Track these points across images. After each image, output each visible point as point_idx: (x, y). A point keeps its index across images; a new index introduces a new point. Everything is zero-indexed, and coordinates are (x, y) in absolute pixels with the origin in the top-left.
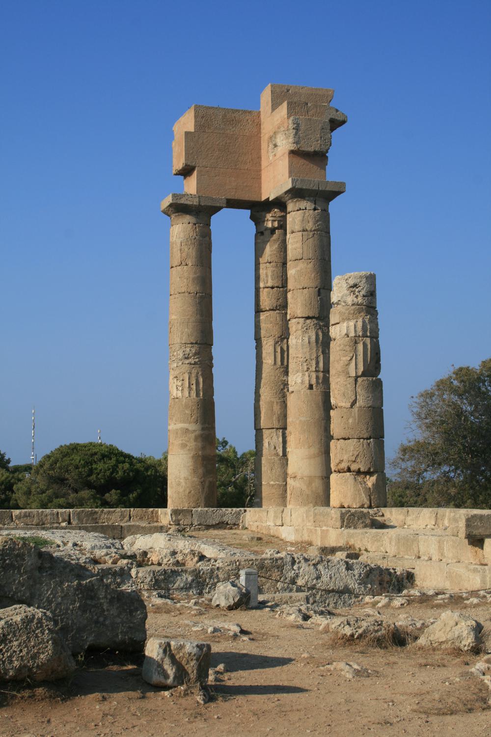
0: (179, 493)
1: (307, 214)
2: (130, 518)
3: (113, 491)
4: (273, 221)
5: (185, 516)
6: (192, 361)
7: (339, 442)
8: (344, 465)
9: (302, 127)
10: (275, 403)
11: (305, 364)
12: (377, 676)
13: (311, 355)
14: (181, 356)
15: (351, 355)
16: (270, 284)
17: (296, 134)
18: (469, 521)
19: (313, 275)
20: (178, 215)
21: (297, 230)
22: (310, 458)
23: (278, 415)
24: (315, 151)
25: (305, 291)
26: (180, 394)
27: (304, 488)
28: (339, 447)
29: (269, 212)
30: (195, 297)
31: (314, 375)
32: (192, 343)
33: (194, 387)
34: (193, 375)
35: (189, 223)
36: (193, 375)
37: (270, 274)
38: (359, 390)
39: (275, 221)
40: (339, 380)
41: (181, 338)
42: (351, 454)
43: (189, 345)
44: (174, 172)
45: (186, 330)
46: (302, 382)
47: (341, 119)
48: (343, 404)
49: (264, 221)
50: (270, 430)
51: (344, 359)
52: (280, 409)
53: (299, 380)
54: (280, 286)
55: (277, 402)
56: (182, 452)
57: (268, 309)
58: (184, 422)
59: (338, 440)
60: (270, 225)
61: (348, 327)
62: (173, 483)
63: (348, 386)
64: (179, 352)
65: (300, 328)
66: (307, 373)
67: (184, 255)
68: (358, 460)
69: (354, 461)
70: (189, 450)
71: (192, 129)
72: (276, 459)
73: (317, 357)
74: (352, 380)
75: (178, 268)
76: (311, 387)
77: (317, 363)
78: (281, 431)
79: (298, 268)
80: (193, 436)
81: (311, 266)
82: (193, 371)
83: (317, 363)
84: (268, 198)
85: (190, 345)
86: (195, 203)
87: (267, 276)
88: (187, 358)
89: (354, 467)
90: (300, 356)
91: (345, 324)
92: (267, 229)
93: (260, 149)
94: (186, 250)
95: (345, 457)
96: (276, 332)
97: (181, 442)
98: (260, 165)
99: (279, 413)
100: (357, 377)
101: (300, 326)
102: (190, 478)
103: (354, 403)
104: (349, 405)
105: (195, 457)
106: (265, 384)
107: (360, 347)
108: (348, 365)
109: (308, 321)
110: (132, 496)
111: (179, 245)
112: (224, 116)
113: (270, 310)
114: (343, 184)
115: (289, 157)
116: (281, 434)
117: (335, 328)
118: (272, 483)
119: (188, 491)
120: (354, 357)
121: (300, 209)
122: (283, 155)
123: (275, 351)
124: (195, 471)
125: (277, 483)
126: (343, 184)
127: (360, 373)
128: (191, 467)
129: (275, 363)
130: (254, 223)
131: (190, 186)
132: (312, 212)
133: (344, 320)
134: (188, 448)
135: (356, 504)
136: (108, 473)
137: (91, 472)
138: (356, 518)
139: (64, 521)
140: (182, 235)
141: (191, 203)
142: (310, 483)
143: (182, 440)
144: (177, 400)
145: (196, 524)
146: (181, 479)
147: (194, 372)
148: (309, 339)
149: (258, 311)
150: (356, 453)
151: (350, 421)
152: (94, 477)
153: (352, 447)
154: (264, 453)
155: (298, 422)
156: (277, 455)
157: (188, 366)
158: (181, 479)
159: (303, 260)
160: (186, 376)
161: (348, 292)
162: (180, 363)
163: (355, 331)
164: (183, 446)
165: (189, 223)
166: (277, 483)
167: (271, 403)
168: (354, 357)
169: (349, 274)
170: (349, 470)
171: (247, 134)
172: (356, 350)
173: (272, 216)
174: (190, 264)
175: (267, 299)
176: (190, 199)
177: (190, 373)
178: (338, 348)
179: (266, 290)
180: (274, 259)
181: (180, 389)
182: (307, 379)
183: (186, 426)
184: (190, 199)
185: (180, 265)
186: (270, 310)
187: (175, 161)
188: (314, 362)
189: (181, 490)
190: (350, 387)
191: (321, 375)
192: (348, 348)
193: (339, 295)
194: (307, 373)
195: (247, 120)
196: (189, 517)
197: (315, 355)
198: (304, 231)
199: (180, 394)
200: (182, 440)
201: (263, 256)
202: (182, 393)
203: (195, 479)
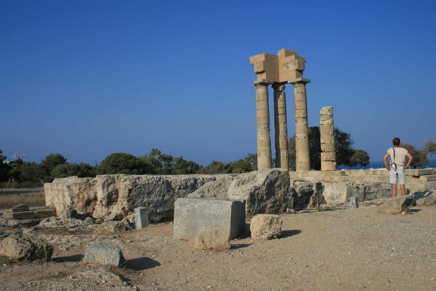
3: (135, 169)
4: (282, 88)
6: (266, 129)
8: (329, 159)
9: (300, 63)
12: (18, 239)
13: (305, 128)
14: (264, 128)
16: (281, 107)
17: (298, 65)
18: (419, 171)
22: (307, 157)
25: (303, 110)
26: (264, 139)
27: (305, 166)
28: (327, 154)
29: (280, 85)
30: (267, 110)
32: (267, 124)
34: (267, 133)
37: (281, 104)
38: (332, 138)
41: (264, 123)
46: (303, 136)
48: (328, 143)
49: (279, 88)
53: (302, 136)
56: (265, 156)
58: (265, 147)
59: (326, 152)
60: (281, 89)
61: (329, 122)
66: (304, 134)
67: (263, 98)
71: (264, 60)
73: (306, 129)
79: (300, 104)
81: (304, 103)
88: (265, 128)
89: (331, 160)
90: (302, 128)
91: (328, 121)
92: (280, 91)
96: (283, 120)
100: (331, 135)
101: (301, 120)
103: (331, 142)
104: (330, 143)
106: (281, 136)
109: (304, 119)
110: (141, 171)
113: (282, 114)
114: (310, 80)
121: (300, 87)
122: (293, 70)
126: (310, 80)
129: (284, 130)
130: (273, 89)
133: (327, 119)
136: (133, 163)
137: (128, 164)
140: (263, 92)
142: (306, 164)
144: (262, 141)
149: (285, 114)
150: (332, 156)
151: (330, 147)
152: (129, 165)
154: (281, 156)
156: (285, 157)
160: (266, 134)
161: (328, 112)
162: (263, 130)
163: (331, 123)
164: (266, 154)
167: (283, 142)
169: (328, 107)
170: (330, 161)
175: (281, 111)
179: (280, 108)
180: (282, 100)
182: (304, 135)
186: (282, 114)
187: (255, 69)
188: (306, 130)
194: (304, 134)
198: (302, 93)
199: (264, 139)
201: (279, 98)
203: (269, 164)
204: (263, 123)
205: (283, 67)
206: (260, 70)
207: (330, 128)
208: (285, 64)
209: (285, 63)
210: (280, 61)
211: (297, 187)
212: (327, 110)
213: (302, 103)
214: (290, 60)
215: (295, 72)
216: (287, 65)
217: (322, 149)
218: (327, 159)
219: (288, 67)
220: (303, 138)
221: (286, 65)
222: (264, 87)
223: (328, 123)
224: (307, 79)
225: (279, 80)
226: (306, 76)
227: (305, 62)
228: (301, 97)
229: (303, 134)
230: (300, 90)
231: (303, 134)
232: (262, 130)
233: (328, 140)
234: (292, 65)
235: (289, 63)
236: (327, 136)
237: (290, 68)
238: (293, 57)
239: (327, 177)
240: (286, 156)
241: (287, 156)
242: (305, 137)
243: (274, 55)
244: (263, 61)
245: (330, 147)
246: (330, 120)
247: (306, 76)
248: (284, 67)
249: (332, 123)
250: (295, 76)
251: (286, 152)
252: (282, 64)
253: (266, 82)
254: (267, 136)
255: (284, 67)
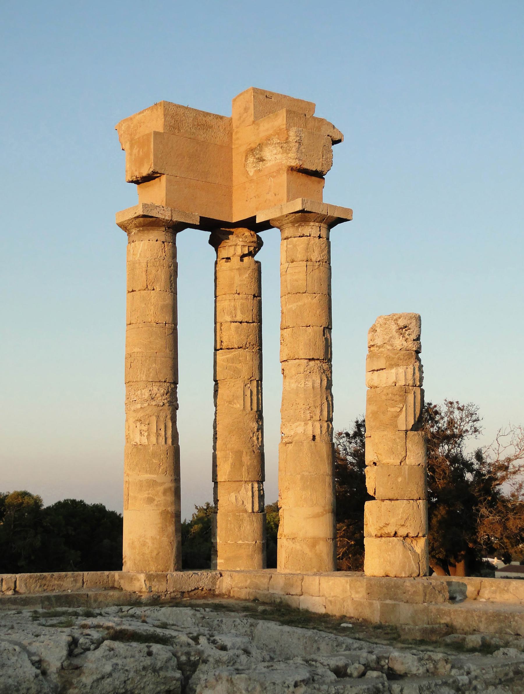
0: (143, 554)
1: (312, 242)
2: (83, 583)
5: (158, 581)
7: (383, 503)
8: (391, 530)
9: (305, 141)
10: (244, 453)
11: (308, 412)
13: (314, 401)
15: (401, 406)
16: (239, 318)
19: (318, 312)
20: (143, 230)
21: (299, 259)
22: (317, 516)
23: (247, 466)
24: (316, 171)
25: (310, 330)
27: (307, 550)
31: (318, 425)
33: (162, 432)
34: (162, 419)
35: (157, 241)
36: (162, 419)
38: (409, 445)
39: (244, 246)
40: (386, 433)
41: (147, 376)
42: (400, 517)
43: (157, 384)
44: (164, 178)
45: (154, 365)
47: (337, 138)
50: (238, 483)
51: (393, 410)
52: (250, 459)
54: (251, 321)
55: (246, 453)
57: (236, 346)
59: (383, 500)
61: (397, 374)
62: (136, 543)
63: (398, 440)
64: (143, 391)
65: (302, 371)
66: (310, 423)
68: (408, 524)
69: (403, 525)
70: (157, 505)
71: (161, 130)
72: (245, 515)
74: (402, 434)
75: (142, 292)
76: (314, 438)
77: (321, 411)
78: (250, 485)
80: (161, 489)
81: (315, 301)
82: (161, 414)
83: (321, 411)
84: (254, 218)
85: (158, 384)
86: (167, 218)
87: (235, 309)
89: (403, 532)
91: (394, 371)
93: (232, 162)
94: (154, 272)
95: (392, 521)
97: (147, 496)
98: (232, 181)
99: (249, 464)
100: (406, 431)
102: (158, 537)
105: (164, 513)
107: (410, 398)
108: (397, 416)
109: (312, 363)
111: (144, 265)
112: (195, 118)
114: (349, 211)
115: (287, 174)
116: (250, 487)
117: (379, 375)
118: (240, 542)
119: (154, 554)
120: (404, 409)
123: (245, 395)
124: (163, 530)
125: (247, 542)
127: (410, 427)
128: (160, 525)
131: (156, 195)
132: (317, 239)
133: (391, 366)
134: (156, 503)
135: (405, 573)
138: (437, 592)
139: (9, 589)
141: (163, 217)
143: (149, 494)
145: (172, 590)
146: (147, 539)
147: (162, 415)
148: (313, 384)
151: (400, 480)
153: (401, 509)
155: (299, 477)
156: (246, 511)
157: (156, 408)
158: (147, 539)
159: (307, 294)
160: (154, 419)
162: (146, 405)
164: (150, 500)
165: (157, 241)
166: (247, 542)
168: (404, 409)
171: (218, 143)
172: (405, 401)
173: (242, 241)
174: (158, 289)
176: (162, 212)
177: (158, 417)
178: (384, 397)
181: (146, 434)
183: (153, 477)
184: (162, 212)
185: (145, 290)
189: (147, 552)
190: (400, 442)
191: (325, 424)
192: (397, 398)
193: (386, 337)
194: (310, 423)
195: (219, 127)
196: (164, 583)
197: (320, 403)
199: (145, 441)
200: (149, 494)
202: (148, 439)
204: (144, 378)
205: (246, 159)
206: (145, 171)
207: (400, 401)
208: (252, 150)
209: (253, 146)
210: (238, 139)
211: (79, 675)
212: (394, 327)
213: (307, 300)
214: (271, 132)
215: (284, 177)
216: (261, 150)
217: (370, 485)
218: (387, 530)
219: (261, 160)
220: (307, 443)
221: (256, 151)
222: (158, 235)
223: (394, 379)
224: (335, 207)
225: (231, 214)
226: (333, 194)
227: (335, 142)
228: (302, 276)
229: (306, 424)
230: (299, 249)
231: (306, 424)
232: (139, 406)
233: (392, 451)
234: (275, 152)
235: (267, 144)
236: (389, 434)
237: (269, 164)
238: (280, 120)
239: (102, 660)
240: (250, 510)
241: (253, 509)
242: (314, 437)
243: (208, 114)
244: (156, 134)
245: (400, 480)
246: (401, 370)
247: (333, 194)
248: (251, 159)
249: (411, 383)
250: (283, 193)
251: (250, 493)
252: (243, 149)
253: (166, 215)
254: (158, 429)
255: (251, 159)
